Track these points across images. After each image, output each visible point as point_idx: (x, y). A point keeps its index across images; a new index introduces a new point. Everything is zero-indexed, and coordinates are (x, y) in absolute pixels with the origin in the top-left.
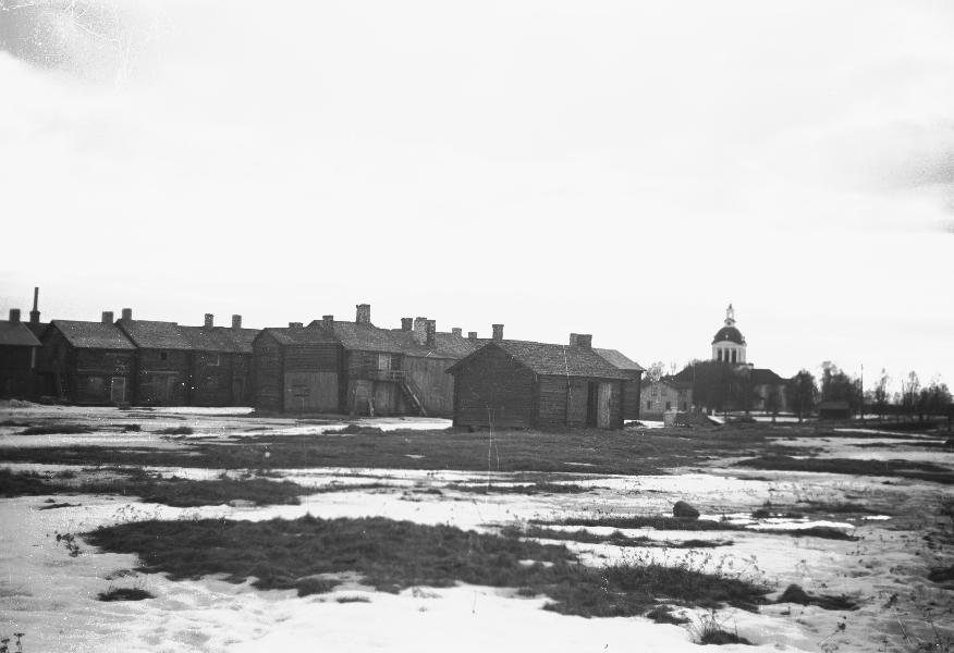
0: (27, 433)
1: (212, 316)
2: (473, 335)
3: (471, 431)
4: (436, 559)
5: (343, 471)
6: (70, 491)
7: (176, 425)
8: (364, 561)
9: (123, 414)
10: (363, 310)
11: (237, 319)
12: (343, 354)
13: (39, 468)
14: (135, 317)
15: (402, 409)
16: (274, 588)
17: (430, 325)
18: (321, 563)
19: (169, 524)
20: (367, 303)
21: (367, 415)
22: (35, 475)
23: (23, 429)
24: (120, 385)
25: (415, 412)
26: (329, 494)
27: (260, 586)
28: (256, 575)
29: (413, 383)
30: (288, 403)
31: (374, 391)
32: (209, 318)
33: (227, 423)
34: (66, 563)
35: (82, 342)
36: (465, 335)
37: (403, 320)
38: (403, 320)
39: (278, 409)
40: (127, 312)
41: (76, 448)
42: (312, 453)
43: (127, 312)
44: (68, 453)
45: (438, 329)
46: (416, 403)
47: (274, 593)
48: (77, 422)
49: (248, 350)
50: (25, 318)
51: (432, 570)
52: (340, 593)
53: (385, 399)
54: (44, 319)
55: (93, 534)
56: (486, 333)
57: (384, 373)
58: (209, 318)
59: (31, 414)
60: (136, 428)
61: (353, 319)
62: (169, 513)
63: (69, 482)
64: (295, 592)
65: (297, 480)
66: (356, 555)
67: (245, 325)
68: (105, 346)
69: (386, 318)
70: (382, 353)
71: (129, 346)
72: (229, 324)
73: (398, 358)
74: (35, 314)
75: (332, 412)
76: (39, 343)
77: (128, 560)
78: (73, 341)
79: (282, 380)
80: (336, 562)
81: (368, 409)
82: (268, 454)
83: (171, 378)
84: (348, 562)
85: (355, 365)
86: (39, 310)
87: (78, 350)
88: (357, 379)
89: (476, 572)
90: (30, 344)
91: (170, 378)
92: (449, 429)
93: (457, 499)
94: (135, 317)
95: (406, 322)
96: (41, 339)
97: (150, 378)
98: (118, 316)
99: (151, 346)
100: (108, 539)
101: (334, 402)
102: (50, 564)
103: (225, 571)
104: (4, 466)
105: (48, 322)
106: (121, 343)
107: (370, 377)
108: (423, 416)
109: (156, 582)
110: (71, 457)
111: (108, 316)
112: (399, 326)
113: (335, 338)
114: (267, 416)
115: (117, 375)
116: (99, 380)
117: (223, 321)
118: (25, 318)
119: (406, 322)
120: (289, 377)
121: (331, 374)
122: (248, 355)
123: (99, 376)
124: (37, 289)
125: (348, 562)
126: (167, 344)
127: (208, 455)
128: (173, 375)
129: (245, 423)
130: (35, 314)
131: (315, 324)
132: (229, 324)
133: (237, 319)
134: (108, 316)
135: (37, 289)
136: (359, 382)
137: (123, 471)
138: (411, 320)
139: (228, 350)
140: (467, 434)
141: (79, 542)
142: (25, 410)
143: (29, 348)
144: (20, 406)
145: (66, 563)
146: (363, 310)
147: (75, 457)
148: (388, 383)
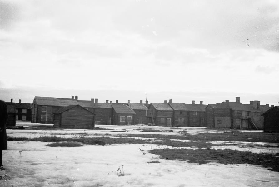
0: (143, 132)
1: (194, 101)
2: (111, 102)
3: (269, 132)
4: (241, 158)
5: (227, 141)
6: (149, 143)
7: (182, 130)
8: (220, 157)
9: (169, 128)
10: (238, 99)
11: (201, 102)
12: (232, 111)
13: (143, 139)
14: (173, 102)
15: (250, 127)
16: (193, 162)
17: (258, 102)
18: (208, 158)
19: (171, 149)
20: (239, 96)
21: (240, 129)
22: (142, 140)
23: (142, 131)
24: (169, 121)
25: (254, 128)
26: (220, 146)
27: (189, 162)
28: (189, 159)
29: (253, 120)
30: (216, 126)
31: (241, 122)
32: (193, 102)
33: (198, 130)
34: (142, 156)
35: (158, 109)
36: (270, 106)
37: (250, 101)
38: (250, 101)
39: (214, 127)
40: (171, 100)
41: (154, 135)
42: (219, 137)
43: (171, 100)
44: (152, 136)
45: (261, 104)
46: (254, 126)
47: (193, 164)
48: (156, 129)
49: (204, 111)
50: (144, 102)
51: (239, 160)
52: (210, 163)
53: (245, 124)
54: (149, 103)
55: (151, 151)
56: (114, 102)
57: (244, 117)
58: (193, 102)
59: (145, 128)
60: (172, 131)
61: (235, 101)
62: (171, 148)
63: (150, 142)
64: (198, 163)
65: (212, 143)
66: (218, 156)
67: (203, 104)
68: (165, 110)
69: (245, 101)
70: (243, 111)
71: (171, 110)
72: (199, 104)
73: (249, 112)
74: (147, 101)
75: (229, 128)
76: (147, 109)
77: (157, 156)
78: (156, 108)
79: (214, 119)
80: (212, 157)
81: (240, 127)
82: (206, 137)
83: (183, 119)
84: (215, 158)
85: (235, 114)
86: (148, 100)
87: (158, 111)
88: (236, 118)
89: (252, 161)
90: (145, 109)
91: (183, 118)
92: (263, 132)
93: (257, 148)
94: (173, 102)
95: (251, 102)
96: (148, 108)
97: (160, 118)
98: (168, 102)
99: (178, 110)
100: (153, 152)
101: (229, 125)
102: (138, 156)
103: (182, 159)
104: (276, 151)
105: (150, 103)
106: (169, 109)
107: (240, 118)
108: (257, 129)
109: (164, 161)
110: (152, 137)
111: (166, 101)
112: (249, 103)
113: (229, 107)
114: (210, 129)
115: (168, 118)
116: (164, 119)
117: (197, 103)
118: (144, 102)
119: (251, 102)
120: (216, 118)
121: (229, 117)
122: (204, 112)
123: (164, 118)
124: (147, 95)
125: (215, 158)
126: (181, 109)
127: (189, 137)
128: (183, 118)
129: (203, 131)
130: (147, 101)
131: (223, 102)
132: (199, 104)
133: (201, 102)
134: (166, 101)
135: (147, 95)
136: (237, 119)
137: (164, 140)
138: (93, 99)
139: (199, 111)
140: (268, 133)
141: (146, 152)
142: (144, 127)
143: (145, 110)
144: (143, 126)
145: (142, 156)
146: (238, 99)
147: (154, 137)
148: (246, 120)
